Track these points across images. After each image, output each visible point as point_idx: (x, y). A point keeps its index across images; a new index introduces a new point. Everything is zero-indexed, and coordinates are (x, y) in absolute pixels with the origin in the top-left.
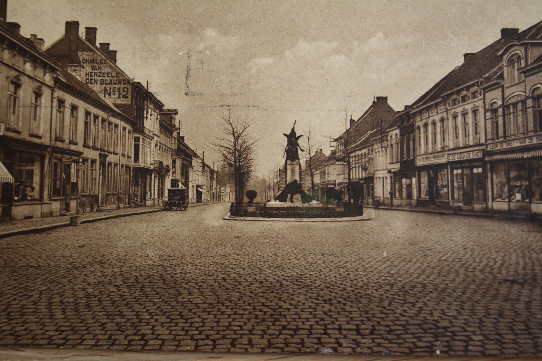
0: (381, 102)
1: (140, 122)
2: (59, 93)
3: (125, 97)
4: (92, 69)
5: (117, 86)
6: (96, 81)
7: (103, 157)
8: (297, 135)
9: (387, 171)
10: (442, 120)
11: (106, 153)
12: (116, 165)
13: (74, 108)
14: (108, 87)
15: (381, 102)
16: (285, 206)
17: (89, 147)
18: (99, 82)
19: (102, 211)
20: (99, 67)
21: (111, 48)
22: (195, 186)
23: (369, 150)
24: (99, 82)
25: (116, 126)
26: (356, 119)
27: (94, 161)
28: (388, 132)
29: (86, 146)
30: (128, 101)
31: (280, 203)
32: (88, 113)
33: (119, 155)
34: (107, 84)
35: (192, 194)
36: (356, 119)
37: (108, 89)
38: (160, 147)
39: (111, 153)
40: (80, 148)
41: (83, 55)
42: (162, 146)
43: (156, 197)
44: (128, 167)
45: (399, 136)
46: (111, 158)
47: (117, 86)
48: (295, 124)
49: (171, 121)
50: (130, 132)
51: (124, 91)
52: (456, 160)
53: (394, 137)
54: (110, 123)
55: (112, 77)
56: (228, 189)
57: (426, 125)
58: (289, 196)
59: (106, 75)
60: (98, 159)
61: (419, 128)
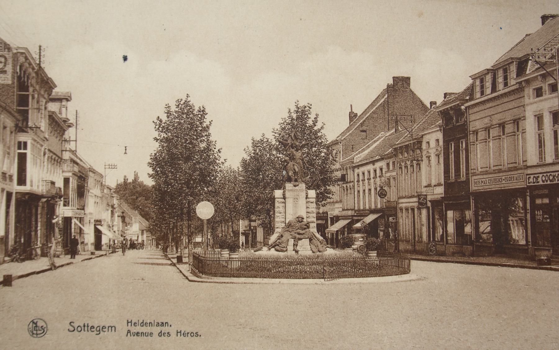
0: (400, 86)
15: (400, 86)
22: (92, 221)
23: (388, 164)
45: (441, 143)
52: (541, 183)
53: (433, 144)
56: (410, 248)
58: (291, 242)
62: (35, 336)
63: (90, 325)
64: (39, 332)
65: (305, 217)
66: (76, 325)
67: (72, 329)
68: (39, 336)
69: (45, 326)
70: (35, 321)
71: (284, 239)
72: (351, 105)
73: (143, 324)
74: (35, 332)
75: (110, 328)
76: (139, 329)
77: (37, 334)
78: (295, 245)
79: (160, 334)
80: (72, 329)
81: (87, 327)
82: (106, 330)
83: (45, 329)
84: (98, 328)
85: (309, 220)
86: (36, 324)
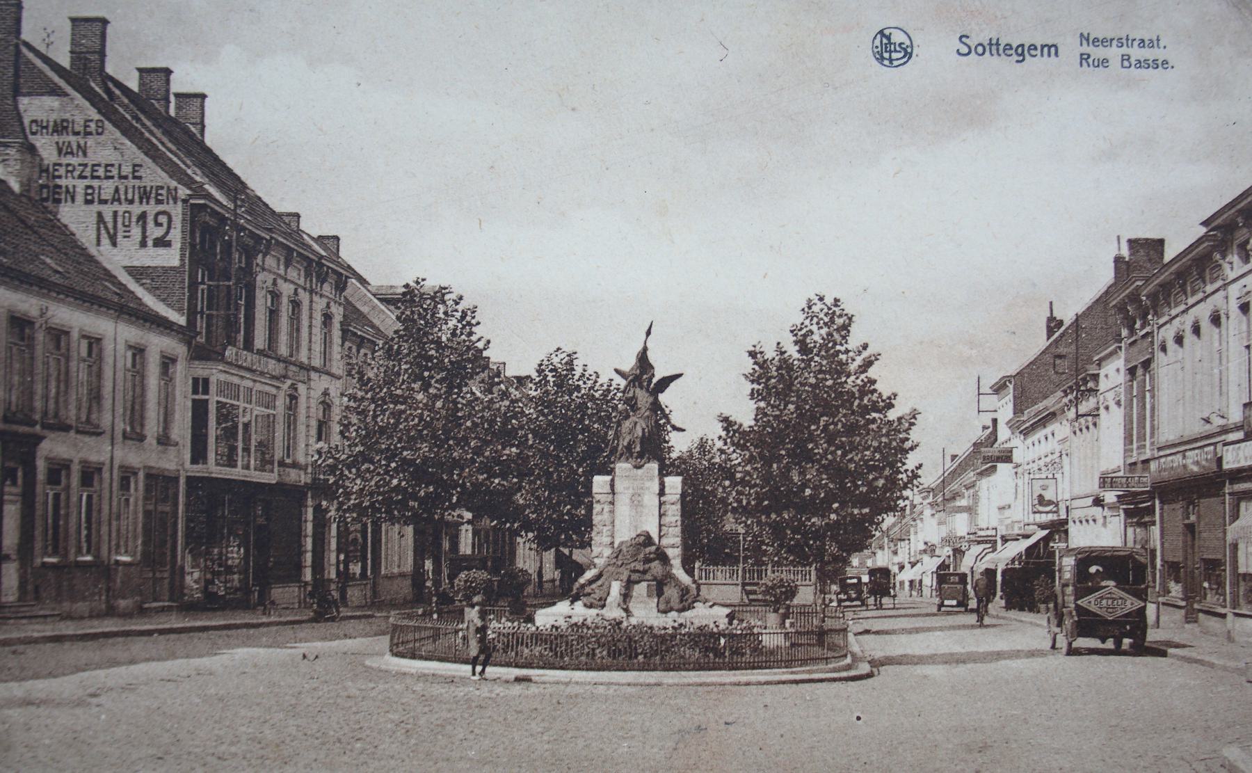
3: (162, 242)
4: (60, 151)
5: (137, 209)
8: (659, 374)
9: (1090, 501)
14: (107, 211)
18: (80, 198)
20: (79, 146)
24: (80, 198)
30: (171, 257)
34: (105, 202)
36: (1067, 315)
47: (137, 209)
48: (648, 333)
51: (158, 224)
58: (616, 588)
62: (886, 62)
63: (1003, 43)
64: (894, 56)
65: (655, 535)
66: (972, 42)
67: (965, 50)
68: (896, 63)
69: (908, 43)
70: (887, 32)
72: (680, 375)
74: (886, 55)
75: (1046, 49)
77: (891, 60)
80: (966, 50)
82: (1039, 52)
84: (1020, 50)
85: (665, 542)
86: (888, 38)
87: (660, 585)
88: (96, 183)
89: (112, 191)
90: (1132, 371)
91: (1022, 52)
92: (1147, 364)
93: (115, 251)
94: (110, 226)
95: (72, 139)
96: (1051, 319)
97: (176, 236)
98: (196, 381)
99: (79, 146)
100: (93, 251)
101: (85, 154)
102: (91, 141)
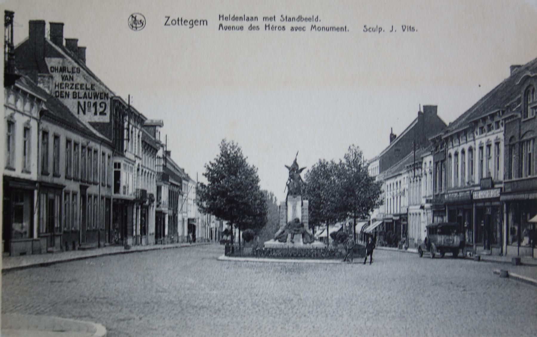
1: (119, 145)
2: (45, 125)
3: (103, 113)
4: (63, 79)
5: (93, 101)
6: (68, 95)
7: (83, 189)
8: (300, 168)
9: (419, 207)
10: (471, 150)
11: (86, 184)
12: (96, 197)
13: (56, 137)
14: (82, 101)
16: (286, 247)
17: (70, 179)
18: (71, 96)
19: (84, 249)
20: (70, 77)
21: (80, 44)
22: (186, 219)
24: (71, 96)
25: (96, 152)
26: (398, 132)
27: (74, 194)
28: (422, 158)
29: (67, 178)
30: (106, 119)
31: (280, 243)
32: (68, 141)
33: (98, 186)
34: (81, 98)
35: (182, 230)
36: (398, 132)
37: (82, 104)
38: (142, 170)
39: (90, 183)
40: (61, 180)
41: (52, 62)
42: (144, 170)
43: (139, 233)
44: (108, 199)
46: (92, 190)
47: (93, 101)
49: (155, 136)
50: (109, 157)
51: (101, 106)
54: (90, 150)
55: (87, 89)
57: (456, 154)
58: (289, 236)
59: (79, 87)
60: (79, 191)
61: (450, 156)
70: (134, 16)
71: (285, 234)
73: (235, 18)
74: (134, 25)
75: (202, 22)
76: (230, 23)
78: (292, 238)
79: (251, 28)
81: (180, 21)
83: (144, 24)
84: (191, 23)
85: (303, 221)
86: (135, 18)
87: (304, 234)
88: (77, 91)
89: (83, 94)
90: (436, 163)
91: (193, 23)
92: (442, 161)
93: (85, 116)
94: (83, 107)
95: (67, 74)
96: (392, 134)
97: (108, 111)
98: (115, 164)
99: (70, 77)
100: (77, 116)
101: (73, 80)
102: (75, 75)
